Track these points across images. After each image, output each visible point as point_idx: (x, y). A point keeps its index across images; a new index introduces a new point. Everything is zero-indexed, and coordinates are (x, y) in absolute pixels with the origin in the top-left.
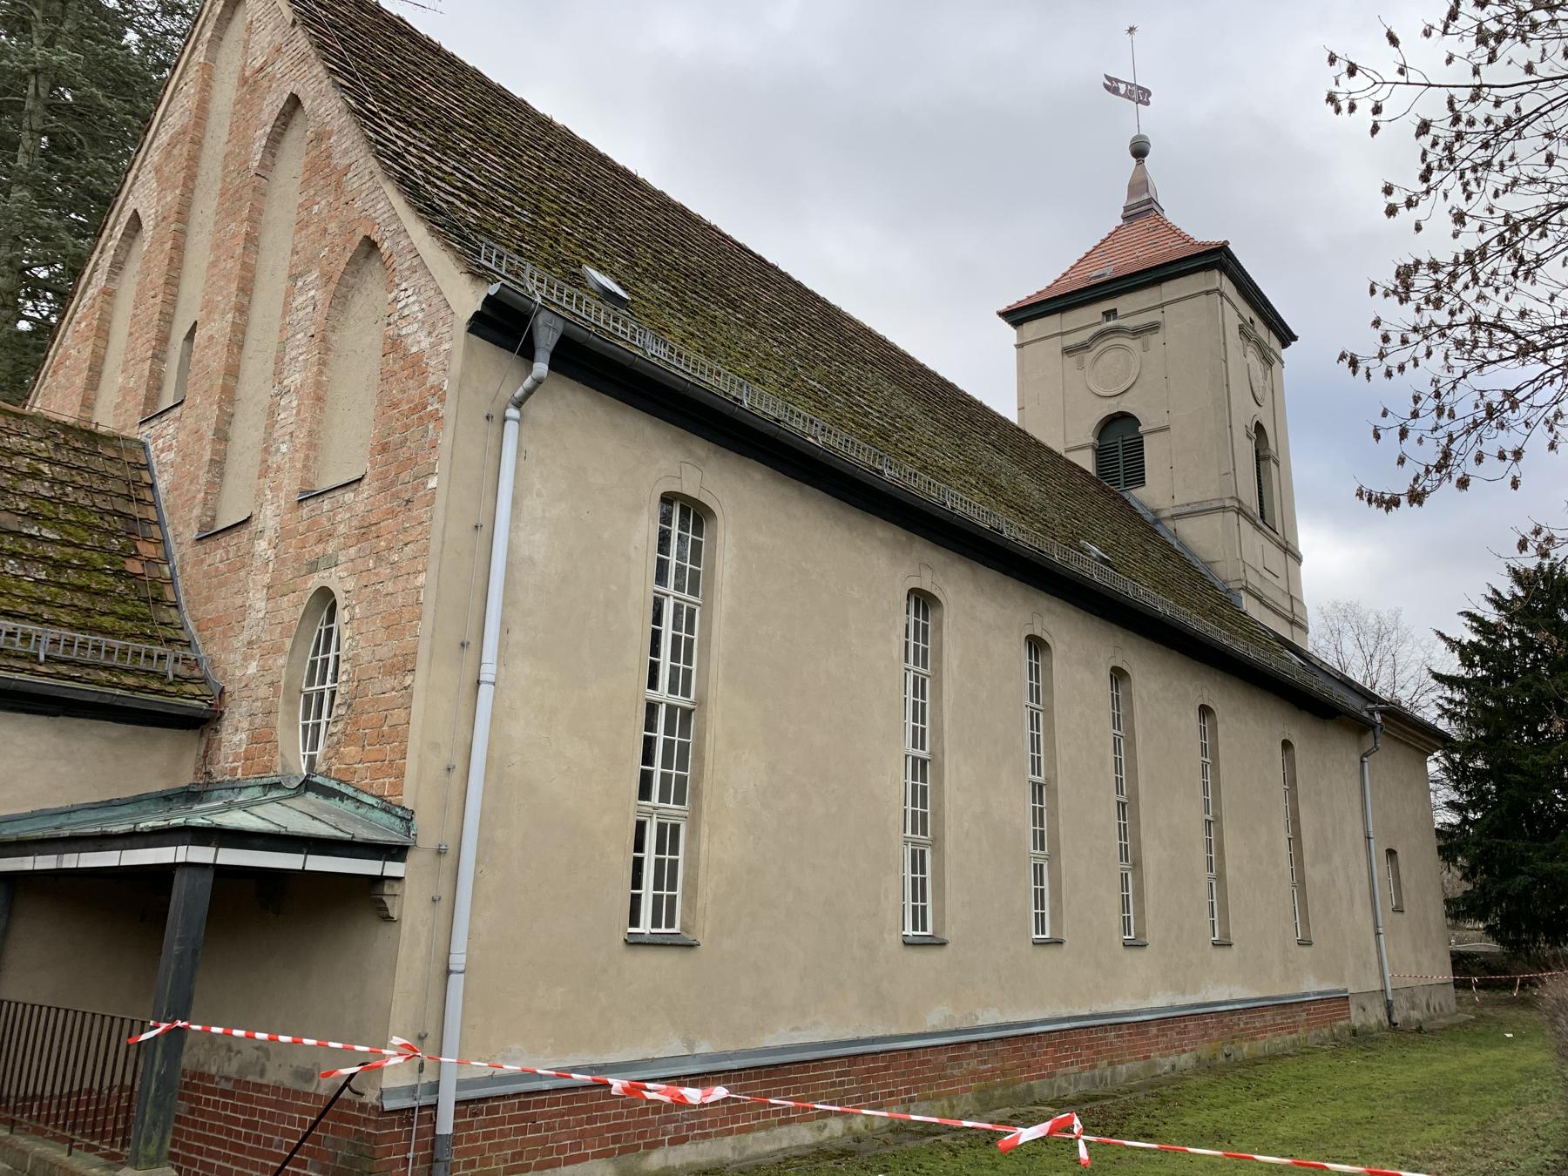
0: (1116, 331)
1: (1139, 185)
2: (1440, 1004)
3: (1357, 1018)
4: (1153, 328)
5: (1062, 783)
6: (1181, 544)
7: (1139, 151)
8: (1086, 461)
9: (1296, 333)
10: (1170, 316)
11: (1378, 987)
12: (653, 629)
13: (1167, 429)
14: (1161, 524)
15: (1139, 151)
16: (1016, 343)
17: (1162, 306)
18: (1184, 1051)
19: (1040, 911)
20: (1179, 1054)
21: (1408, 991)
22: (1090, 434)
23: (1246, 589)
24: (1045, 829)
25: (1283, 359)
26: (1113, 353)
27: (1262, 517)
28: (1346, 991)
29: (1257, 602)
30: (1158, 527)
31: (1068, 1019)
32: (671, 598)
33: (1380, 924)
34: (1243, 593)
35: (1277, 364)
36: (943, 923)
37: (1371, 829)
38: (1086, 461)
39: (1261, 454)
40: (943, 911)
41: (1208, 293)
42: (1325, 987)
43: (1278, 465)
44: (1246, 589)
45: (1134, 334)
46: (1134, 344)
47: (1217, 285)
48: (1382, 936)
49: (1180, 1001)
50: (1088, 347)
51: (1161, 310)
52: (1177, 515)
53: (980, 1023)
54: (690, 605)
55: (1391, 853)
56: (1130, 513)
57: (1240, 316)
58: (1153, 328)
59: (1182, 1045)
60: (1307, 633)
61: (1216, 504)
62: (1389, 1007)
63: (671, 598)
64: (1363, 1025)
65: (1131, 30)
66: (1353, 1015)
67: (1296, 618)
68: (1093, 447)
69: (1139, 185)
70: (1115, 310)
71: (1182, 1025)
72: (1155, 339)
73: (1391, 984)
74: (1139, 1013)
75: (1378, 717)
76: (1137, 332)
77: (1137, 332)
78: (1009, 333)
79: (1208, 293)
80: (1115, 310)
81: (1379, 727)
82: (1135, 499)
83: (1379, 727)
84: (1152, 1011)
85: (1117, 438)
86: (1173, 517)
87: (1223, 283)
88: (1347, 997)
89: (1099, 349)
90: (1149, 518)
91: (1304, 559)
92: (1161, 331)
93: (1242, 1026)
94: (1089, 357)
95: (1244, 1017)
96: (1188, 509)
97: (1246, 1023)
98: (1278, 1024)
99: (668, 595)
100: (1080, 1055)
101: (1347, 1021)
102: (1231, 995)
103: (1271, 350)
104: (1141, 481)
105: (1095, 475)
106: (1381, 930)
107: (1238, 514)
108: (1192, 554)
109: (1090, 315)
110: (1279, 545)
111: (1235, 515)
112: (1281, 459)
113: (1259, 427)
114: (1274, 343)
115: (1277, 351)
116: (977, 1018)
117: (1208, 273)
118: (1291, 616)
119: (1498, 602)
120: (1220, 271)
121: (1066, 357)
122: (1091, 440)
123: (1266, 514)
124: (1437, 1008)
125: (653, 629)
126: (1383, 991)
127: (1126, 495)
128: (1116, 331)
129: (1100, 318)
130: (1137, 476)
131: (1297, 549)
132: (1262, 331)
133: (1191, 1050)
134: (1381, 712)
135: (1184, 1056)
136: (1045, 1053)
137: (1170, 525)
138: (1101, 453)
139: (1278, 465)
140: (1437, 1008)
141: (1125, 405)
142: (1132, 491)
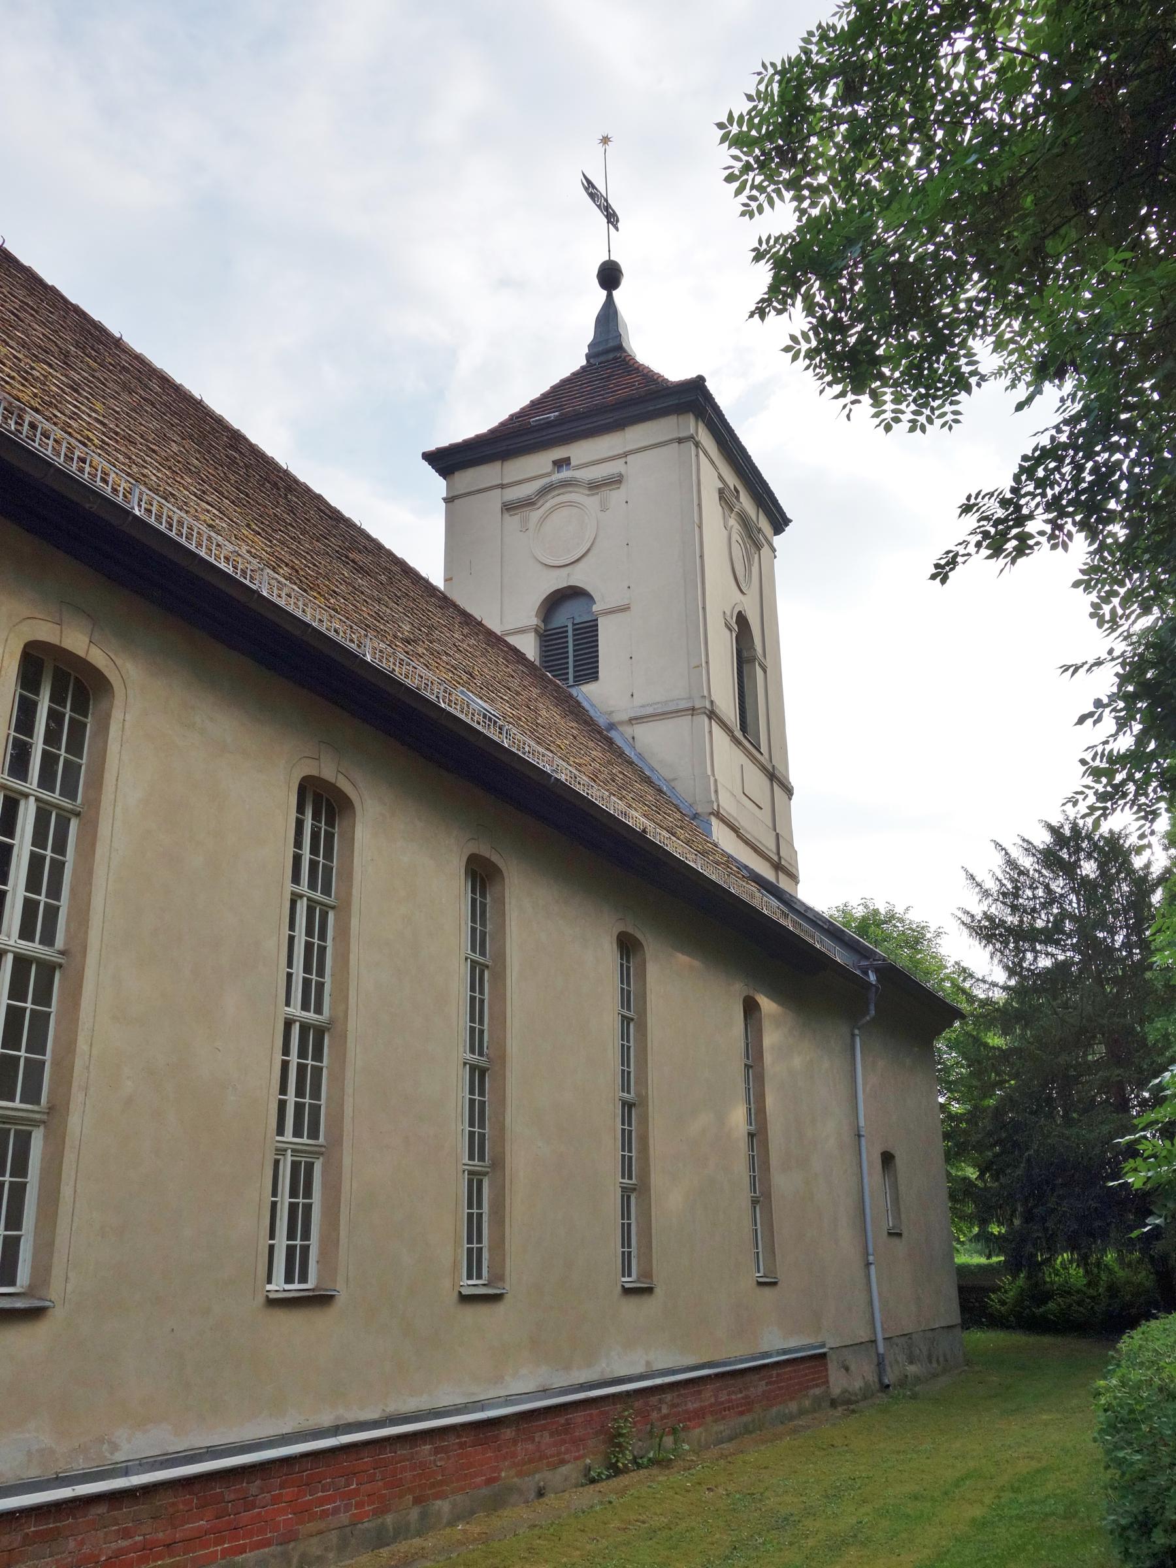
0: (566, 484)
1: (608, 318)
2: (945, 1356)
3: (838, 1382)
4: (616, 481)
5: (356, 1025)
6: (639, 755)
7: (610, 276)
8: (529, 646)
9: (789, 516)
10: (634, 468)
11: (863, 1335)
12: (290, 935)
13: (625, 609)
14: (617, 729)
15: (610, 276)
16: (445, 495)
17: (626, 455)
18: (563, 1462)
19: (475, 1211)
20: (554, 1467)
21: (903, 1339)
22: (534, 613)
23: (717, 815)
24: (323, 1102)
25: (775, 545)
26: (565, 512)
27: (744, 728)
28: (823, 1346)
29: (733, 835)
30: (613, 734)
31: (336, 1430)
32: (32, 799)
33: (871, 1251)
34: (714, 821)
35: (765, 550)
36: (48, 1269)
37: (862, 1123)
38: (529, 646)
39: (745, 654)
40: (51, 1244)
41: (680, 441)
42: (792, 1343)
43: (765, 672)
44: (717, 815)
45: (590, 488)
46: (591, 502)
47: (692, 431)
48: (873, 1268)
49: (560, 1380)
50: (533, 504)
51: (623, 460)
52: (636, 719)
53: (119, 1456)
54: (9, 793)
55: (887, 1159)
56: (576, 711)
57: (720, 477)
58: (616, 481)
59: (559, 1454)
60: (797, 883)
61: (684, 705)
62: (880, 1364)
63: (32, 799)
64: (845, 1391)
65: (605, 140)
66: (832, 1379)
67: (783, 863)
68: (536, 631)
69: (608, 318)
70: (569, 459)
71: (562, 1420)
72: (616, 497)
73: (883, 1329)
74: (481, 1406)
75: (872, 978)
76: (595, 487)
77: (595, 487)
78: (439, 485)
79: (680, 441)
80: (569, 459)
81: (874, 989)
82: (587, 699)
83: (874, 989)
84: (508, 1400)
85: (565, 617)
86: (633, 721)
87: (700, 430)
88: (824, 1355)
89: (548, 505)
90: (602, 721)
91: (795, 791)
92: (623, 487)
93: (665, 1411)
94: (535, 515)
95: (668, 1397)
96: (650, 711)
97: (674, 1406)
98: (722, 1403)
99: (26, 796)
100: (356, 1492)
101: (823, 1388)
102: (648, 1363)
103: (760, 530)
104: (593, 676)
105: (537, 663)
106: (871, 1258)
107: (710, 718)
108: (652, 769)
109: (538, 464)
110: (763, 768)
111: (706, 720)
112: (769, 663)
113: (742, 620)
114: (764, 525)
115: (769, 537)
116: (115, 1447)
117: (681, 418)
118: (776, 858)
119: (1029, 847)
120: (697, 417)
121: (506, 516)
122: (534, 621)
123: (750, 728)
124: (941, 1359)
125: (290, 935)
126: (874, 1342)
127: (574, 692)
128: (566, 484)
129: (549, 467)
130: (589, 670)
131: (788, 780)
132: (746, 502)
133: (577, 1458)
134: (877, 971)
135: (564, 1470)
136: (276, 1500)
137: (628, 731)
138: (549, 639)
139: (765, 672)
140: (941, 1359)
141: (578, 578)
142: (581, 687)
